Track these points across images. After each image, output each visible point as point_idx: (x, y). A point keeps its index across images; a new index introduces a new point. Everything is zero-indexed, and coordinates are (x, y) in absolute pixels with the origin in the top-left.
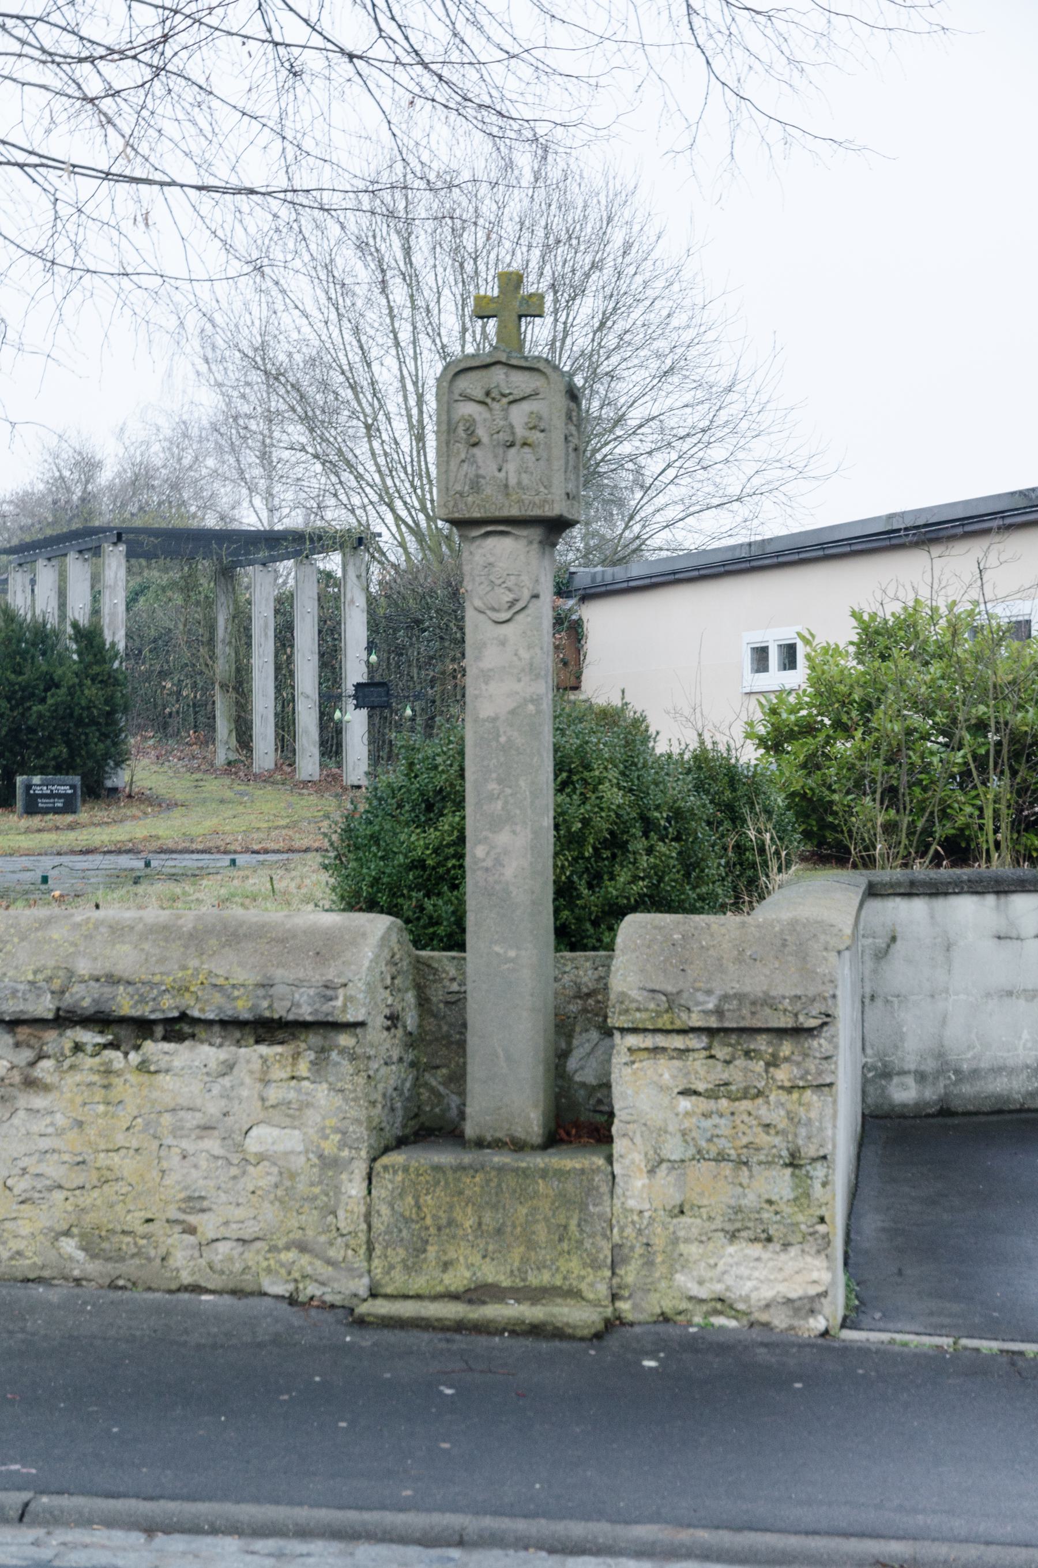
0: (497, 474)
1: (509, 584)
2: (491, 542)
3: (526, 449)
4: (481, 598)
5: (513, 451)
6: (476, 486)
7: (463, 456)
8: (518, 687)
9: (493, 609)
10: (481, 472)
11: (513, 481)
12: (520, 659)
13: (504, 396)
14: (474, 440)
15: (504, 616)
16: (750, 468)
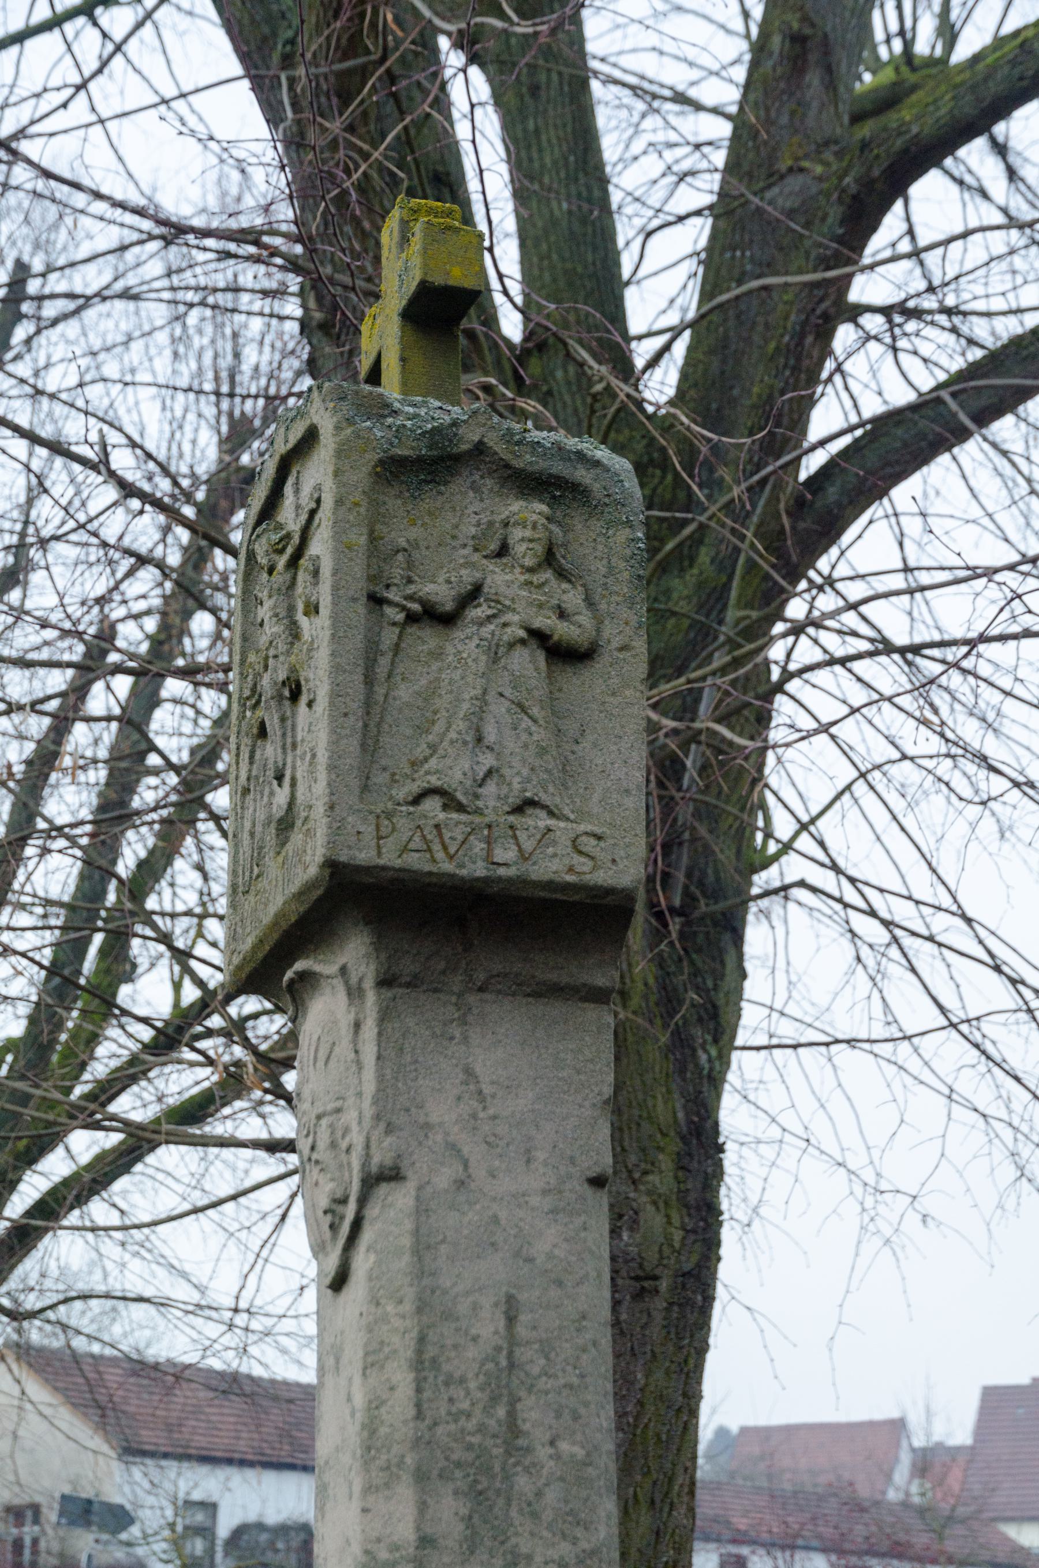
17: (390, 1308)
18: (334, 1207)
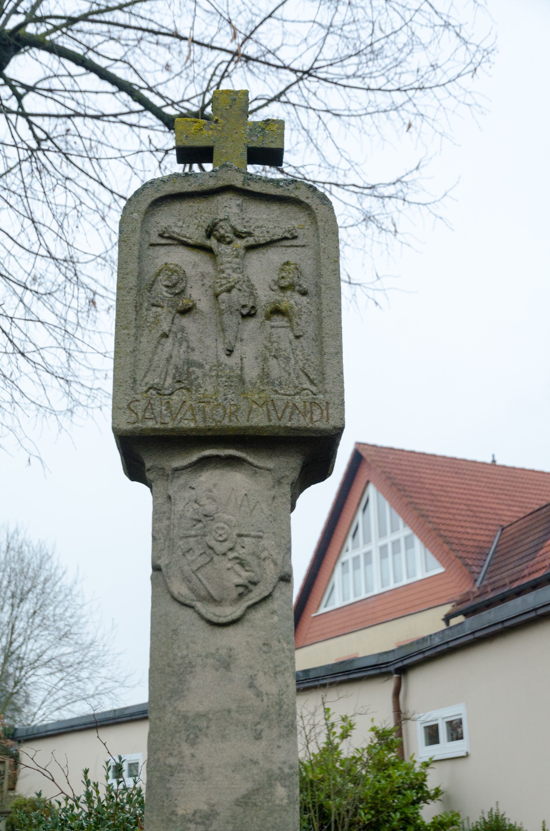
0: (223, 358)
1: (240, 552)
2: (207, 478)
3: (278, 321)
4: (186, 580)
5: (252, 323)
6: (184, 379)
7: (165, 327)
8: (256, 750)
9: (211, 600)
10: (196, 357)
11: (252, 373)
12: (259, 695)
13: (239, 235)
14: (182, 303)
15: (230, 612)
16: (98, 682)
17: (285, 645)
18: (248, 585)
